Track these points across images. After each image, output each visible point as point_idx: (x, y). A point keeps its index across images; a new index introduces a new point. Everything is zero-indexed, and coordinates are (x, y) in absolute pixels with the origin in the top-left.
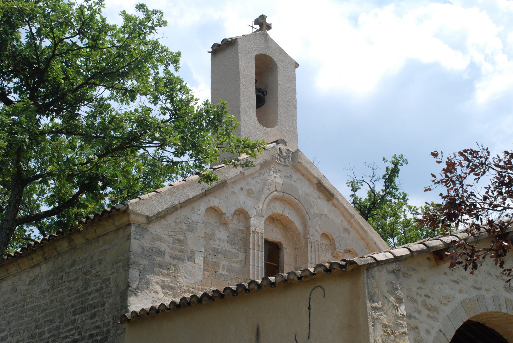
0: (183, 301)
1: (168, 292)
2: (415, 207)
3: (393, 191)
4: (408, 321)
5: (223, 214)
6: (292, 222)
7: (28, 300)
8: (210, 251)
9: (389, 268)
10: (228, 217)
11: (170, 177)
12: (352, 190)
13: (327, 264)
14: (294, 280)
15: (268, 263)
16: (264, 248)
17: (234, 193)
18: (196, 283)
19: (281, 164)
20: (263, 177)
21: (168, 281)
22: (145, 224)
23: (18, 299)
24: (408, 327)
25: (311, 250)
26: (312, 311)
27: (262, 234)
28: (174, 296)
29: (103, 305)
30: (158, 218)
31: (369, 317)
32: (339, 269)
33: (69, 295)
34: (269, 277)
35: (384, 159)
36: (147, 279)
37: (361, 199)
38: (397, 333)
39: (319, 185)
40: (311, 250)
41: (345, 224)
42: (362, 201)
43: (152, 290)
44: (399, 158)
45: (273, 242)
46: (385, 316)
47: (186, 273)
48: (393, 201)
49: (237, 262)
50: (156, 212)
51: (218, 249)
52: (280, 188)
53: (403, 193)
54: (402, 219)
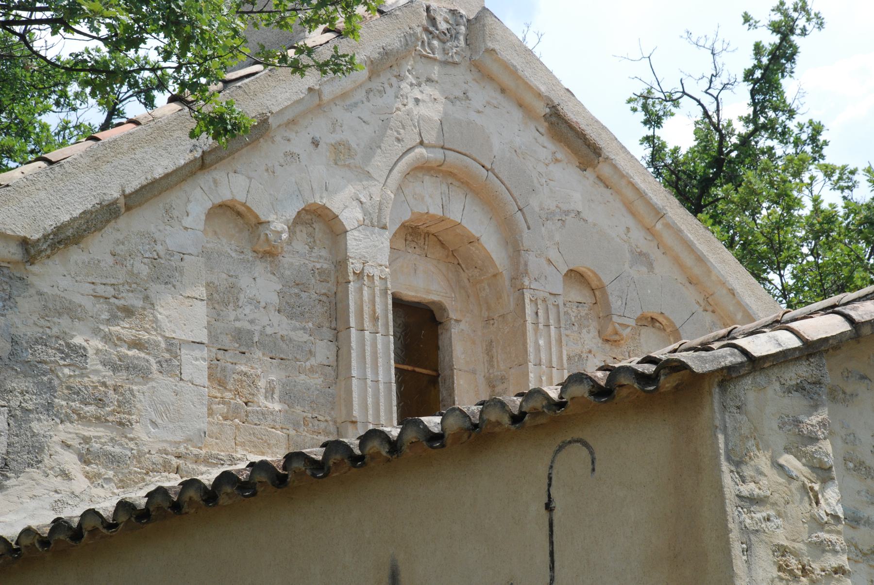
0: (159, 500)
1: (103, 471)
2: (844, 168)
3: (777, 118)
4: (851, 533)
5: (260, 223)
6: (473, 241)
8: (226, 341)
9: (787, 376)
10: (279, 233)
11: (61, 97)
12: (645, 123)
13: (600, 374)
14: (499, 423)
15: (405, 367)
16: (391, 323)
17: (292, 156)
18: (189, 440)
19: (435, 59)
20: (378, 101)
21: (100, 437)
22: (17, 263)
24: (850, 552)
25: (536, 324)
26: (557, 515)
27: (385, 279)
28: (123, 484)
30: (59, 242)
31: (731, 526)
32: (636, 386)
34: (422, 418)
35: (747, 19)
36: (34, 435)
37: (676, 150)
38: (818, 571)
39: (554, 119)
40: (536, 324)
41: (638, 237)
42: (681, 158)
43: (52, 468)
44: (795, 10)
45: (418, 303)
46: (779, 521)
47: (156, 410)
48: (779, 150)
49: (312, 370)
50: (49, 224)
51: (250, 333)
52: (434, 134)
53: (811, 123)
54: (806, 210)
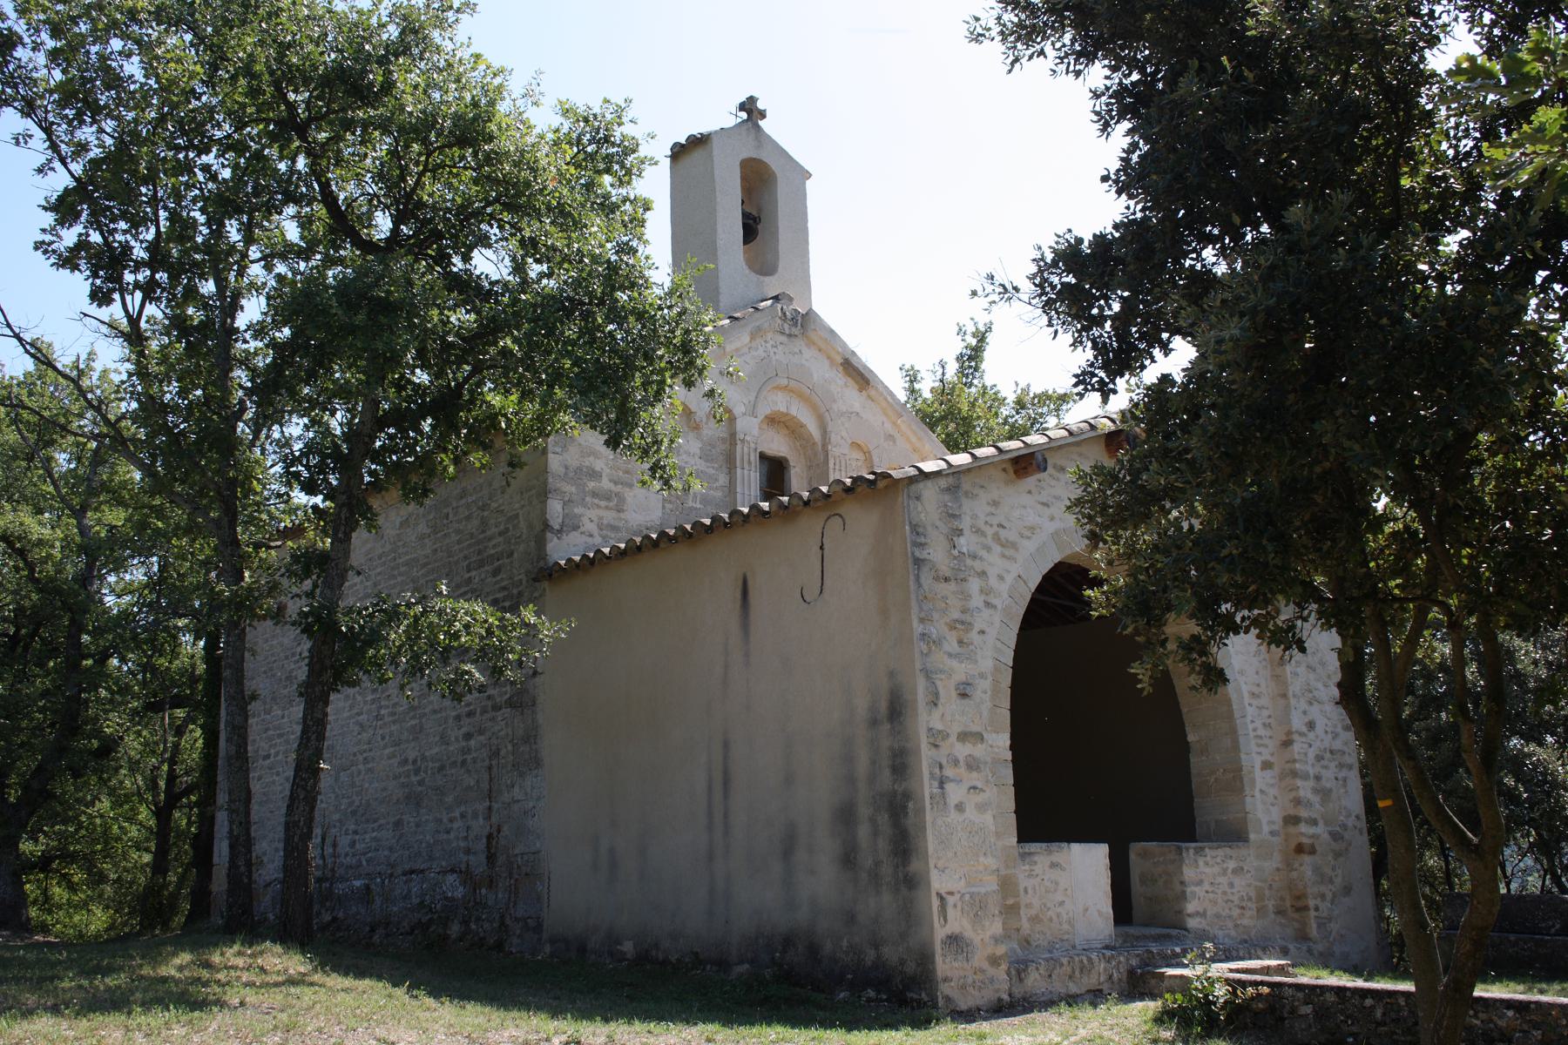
6: (802, 426)
7: (400, 551)
23: (386, 550)
26: (826, 552)
29: (511, 554)
33: (459, 542)
41: (888, 426)
